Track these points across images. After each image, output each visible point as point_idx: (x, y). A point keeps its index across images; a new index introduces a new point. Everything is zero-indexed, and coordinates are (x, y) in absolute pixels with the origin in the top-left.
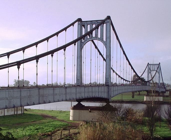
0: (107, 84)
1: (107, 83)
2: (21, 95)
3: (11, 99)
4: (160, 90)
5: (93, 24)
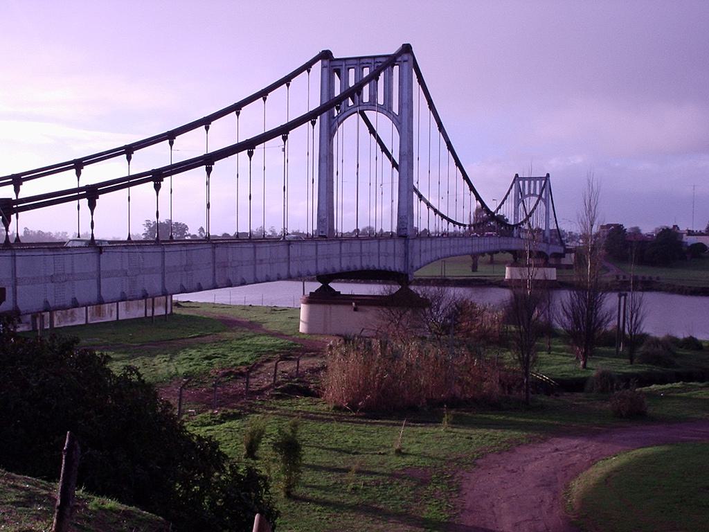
0: (402, 234)
4: (548, 249)
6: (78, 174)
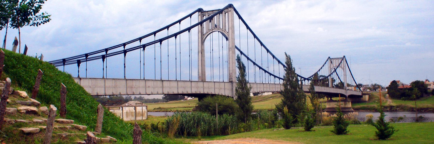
0: (231, 81)
1: (230, 79)
2: (105, 85)
3: (94, 88)
4: (346, 93)
5: (226, 12)
6: (140, 41)
